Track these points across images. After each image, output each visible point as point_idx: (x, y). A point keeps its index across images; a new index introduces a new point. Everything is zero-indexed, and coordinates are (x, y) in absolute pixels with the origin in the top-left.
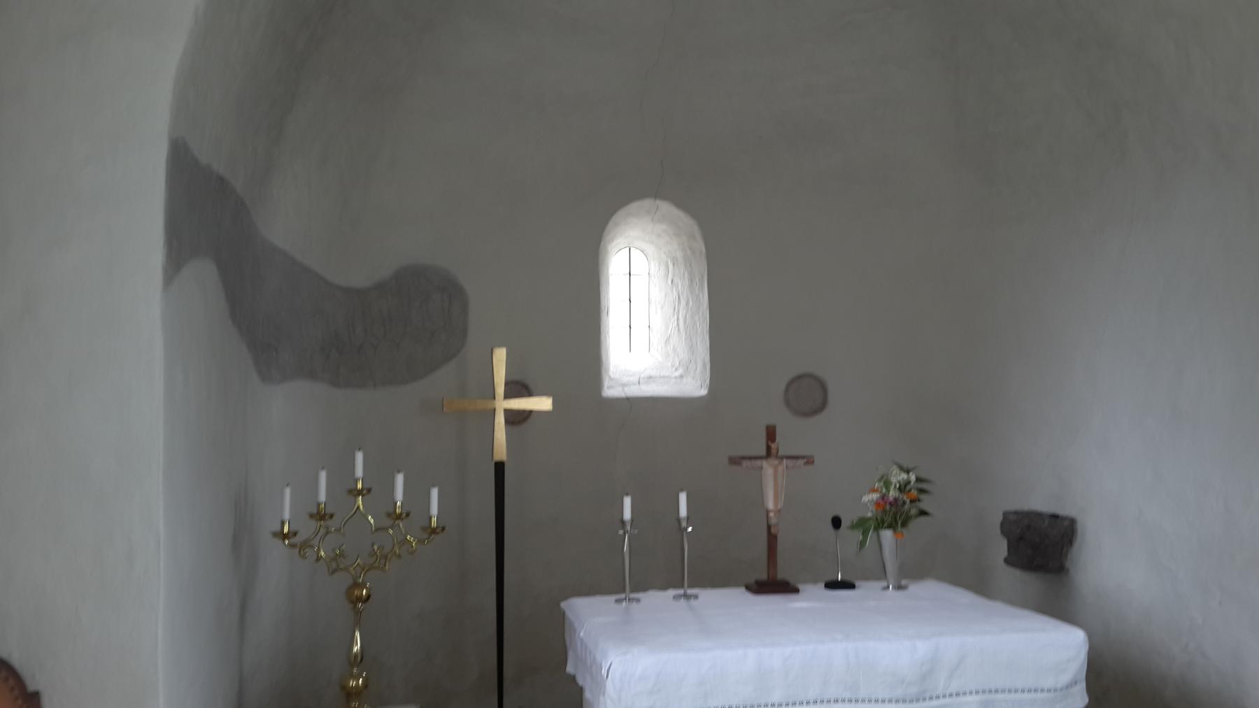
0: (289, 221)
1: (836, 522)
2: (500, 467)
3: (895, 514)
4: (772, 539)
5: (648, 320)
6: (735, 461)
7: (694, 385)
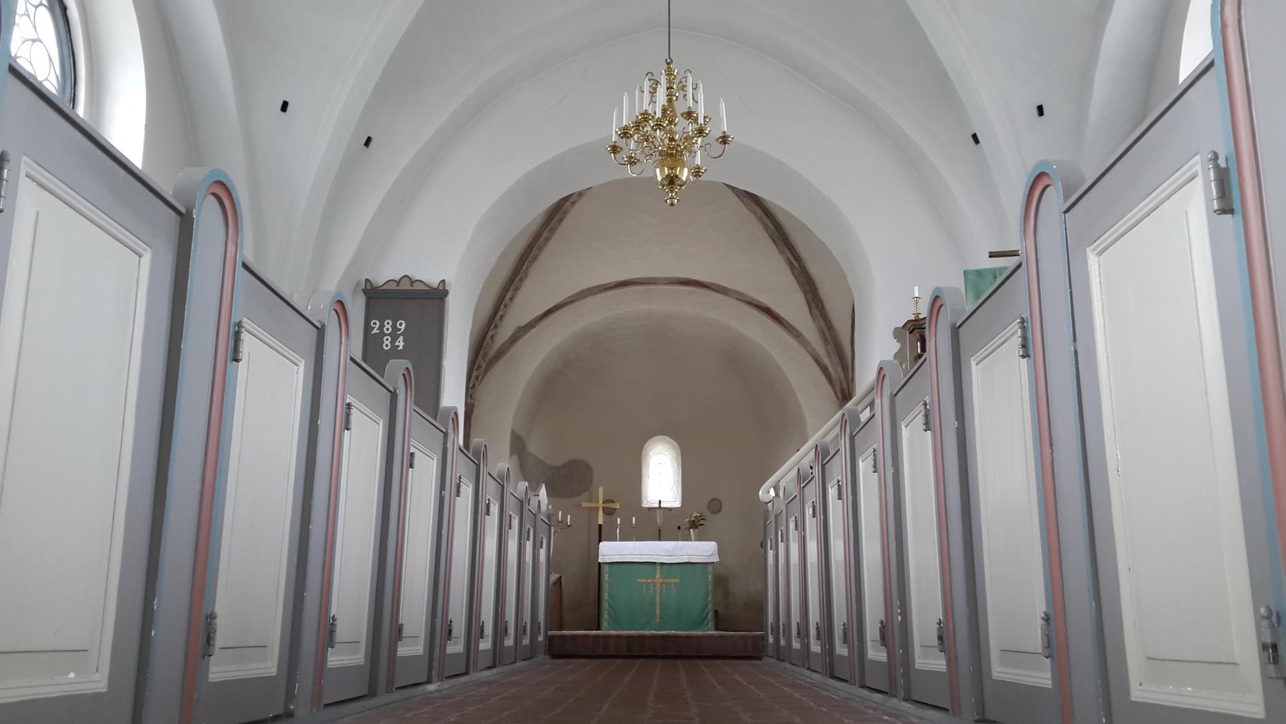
0: (535, 447)
5: (662, 478)
7: (677, 504)
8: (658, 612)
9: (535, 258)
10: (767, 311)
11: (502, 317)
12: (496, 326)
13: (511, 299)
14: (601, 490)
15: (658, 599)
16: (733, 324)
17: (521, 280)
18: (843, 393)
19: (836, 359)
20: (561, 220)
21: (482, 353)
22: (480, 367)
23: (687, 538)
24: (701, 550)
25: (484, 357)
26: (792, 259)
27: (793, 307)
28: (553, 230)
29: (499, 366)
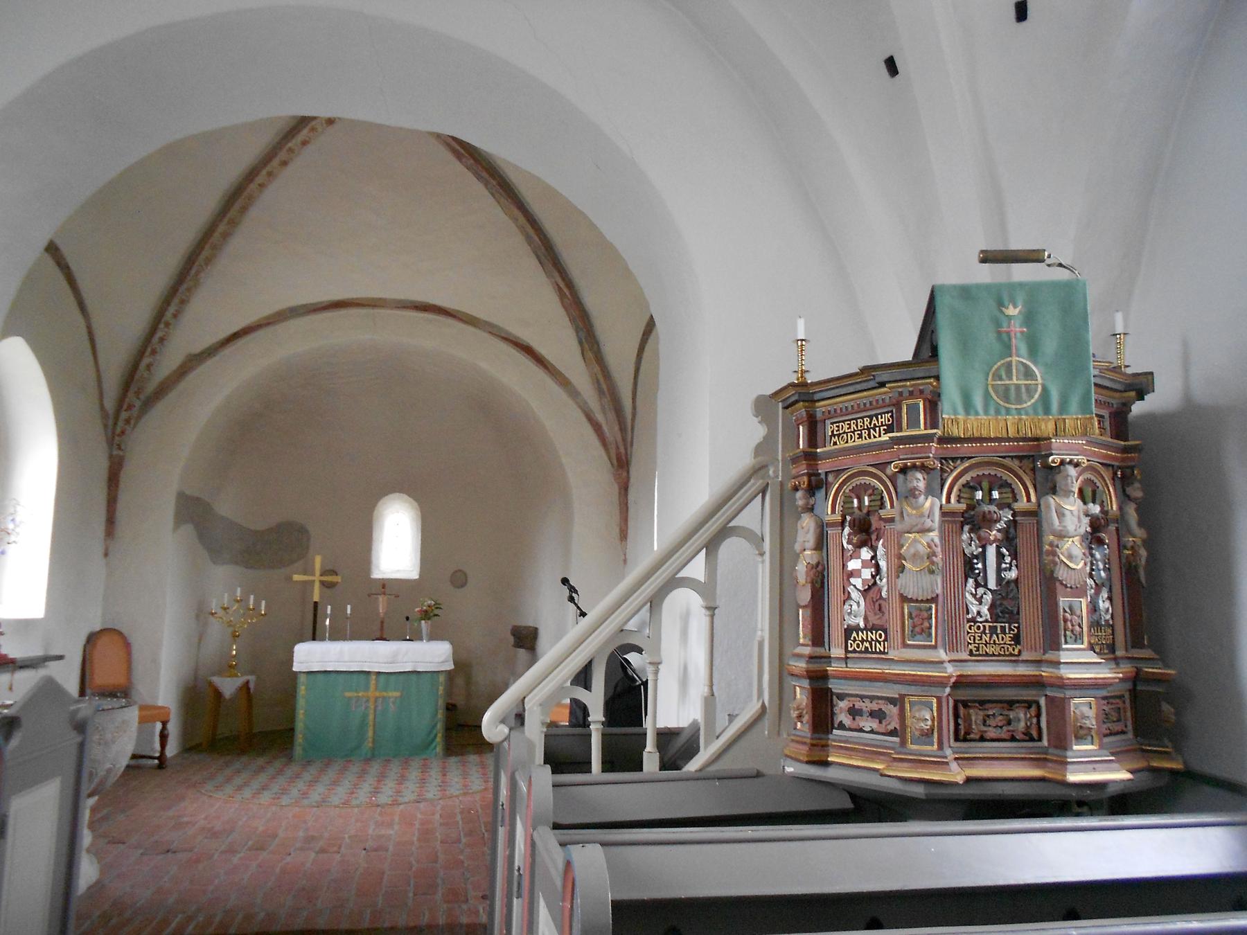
0: (227, 506)
1: (407, 619)
2: (316, 603)
3: (426, 615)
4: (382, 622)
5: (397, 544)
6: (11, 689)
7: (414, 575)
8: (370, 734)
9: (208, 261)
10: (528, 350)
11: (162, 340)
12: (154, 352)
13: (175, 316)
14: (318, 560)
15: (371, 717)
16: (484, 365)
17: (189, 290)
18: (619, 459)
19: (612, 416)
20: (244, 210)
21: (133, 389)
22: (130, 407)
23: (415, 637)
24: (431, 655)
25: (137, 393)
26: (562, 285)
27: (560, 343)
28: (234, 223)
29: (160, 407)
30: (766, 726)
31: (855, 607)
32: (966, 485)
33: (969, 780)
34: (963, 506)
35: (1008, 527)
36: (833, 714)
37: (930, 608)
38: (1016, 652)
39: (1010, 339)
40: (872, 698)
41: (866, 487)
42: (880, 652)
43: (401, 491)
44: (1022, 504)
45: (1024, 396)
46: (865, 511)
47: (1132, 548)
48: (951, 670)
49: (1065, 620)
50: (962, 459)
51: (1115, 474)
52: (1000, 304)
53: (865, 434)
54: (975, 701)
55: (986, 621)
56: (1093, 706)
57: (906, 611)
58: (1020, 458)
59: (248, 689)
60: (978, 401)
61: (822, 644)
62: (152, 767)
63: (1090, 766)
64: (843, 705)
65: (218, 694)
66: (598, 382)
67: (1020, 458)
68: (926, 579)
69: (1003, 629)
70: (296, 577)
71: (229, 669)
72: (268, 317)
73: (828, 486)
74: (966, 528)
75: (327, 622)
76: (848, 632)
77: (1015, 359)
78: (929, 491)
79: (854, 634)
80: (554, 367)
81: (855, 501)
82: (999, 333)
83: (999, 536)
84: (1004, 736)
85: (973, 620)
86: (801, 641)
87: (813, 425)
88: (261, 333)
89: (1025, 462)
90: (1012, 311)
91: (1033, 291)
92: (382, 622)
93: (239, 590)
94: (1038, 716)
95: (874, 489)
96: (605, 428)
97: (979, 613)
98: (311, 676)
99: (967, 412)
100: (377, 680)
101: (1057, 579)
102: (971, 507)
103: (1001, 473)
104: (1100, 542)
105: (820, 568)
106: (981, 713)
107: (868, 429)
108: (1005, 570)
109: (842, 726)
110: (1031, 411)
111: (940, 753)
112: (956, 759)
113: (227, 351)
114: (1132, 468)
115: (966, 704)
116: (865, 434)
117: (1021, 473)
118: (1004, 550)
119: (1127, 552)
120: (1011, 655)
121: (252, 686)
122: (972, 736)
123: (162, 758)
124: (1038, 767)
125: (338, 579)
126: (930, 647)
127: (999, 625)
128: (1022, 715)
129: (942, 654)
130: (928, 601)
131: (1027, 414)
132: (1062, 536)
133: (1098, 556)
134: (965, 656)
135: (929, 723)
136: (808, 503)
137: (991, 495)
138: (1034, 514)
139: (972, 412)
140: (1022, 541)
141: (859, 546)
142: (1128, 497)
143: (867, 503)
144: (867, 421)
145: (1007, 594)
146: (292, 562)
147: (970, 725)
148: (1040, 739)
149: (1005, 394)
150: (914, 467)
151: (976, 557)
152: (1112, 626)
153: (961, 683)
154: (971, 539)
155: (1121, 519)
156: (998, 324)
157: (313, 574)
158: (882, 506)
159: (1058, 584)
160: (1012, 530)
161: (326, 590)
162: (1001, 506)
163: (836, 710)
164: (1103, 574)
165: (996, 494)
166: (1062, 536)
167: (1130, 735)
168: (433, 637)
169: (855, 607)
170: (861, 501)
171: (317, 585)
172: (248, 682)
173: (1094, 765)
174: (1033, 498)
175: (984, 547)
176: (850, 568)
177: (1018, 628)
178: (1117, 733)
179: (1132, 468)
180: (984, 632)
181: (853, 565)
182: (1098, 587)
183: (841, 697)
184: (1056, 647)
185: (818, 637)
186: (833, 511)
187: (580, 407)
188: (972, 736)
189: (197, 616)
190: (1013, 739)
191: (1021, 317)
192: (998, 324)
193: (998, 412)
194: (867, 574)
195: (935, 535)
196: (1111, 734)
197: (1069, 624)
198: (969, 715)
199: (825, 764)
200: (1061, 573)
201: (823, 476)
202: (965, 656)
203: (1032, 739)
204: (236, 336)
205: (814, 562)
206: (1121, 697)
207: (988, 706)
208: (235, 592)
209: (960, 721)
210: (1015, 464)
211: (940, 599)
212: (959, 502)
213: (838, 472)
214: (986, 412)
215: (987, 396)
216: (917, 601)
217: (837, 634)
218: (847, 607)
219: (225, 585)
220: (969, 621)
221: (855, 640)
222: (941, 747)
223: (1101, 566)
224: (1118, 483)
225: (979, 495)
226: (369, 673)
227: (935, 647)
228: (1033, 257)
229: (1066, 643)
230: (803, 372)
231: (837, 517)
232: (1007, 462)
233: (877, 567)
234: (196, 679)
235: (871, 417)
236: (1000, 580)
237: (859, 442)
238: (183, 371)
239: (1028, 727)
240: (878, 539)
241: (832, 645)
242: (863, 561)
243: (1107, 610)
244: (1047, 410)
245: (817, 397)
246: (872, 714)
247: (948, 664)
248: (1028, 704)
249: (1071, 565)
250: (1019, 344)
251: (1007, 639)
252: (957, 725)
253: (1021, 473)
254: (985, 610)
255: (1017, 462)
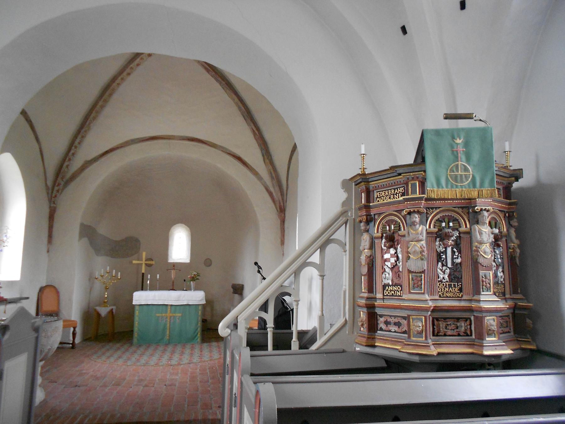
0: (103, 230)
1: (185, 280)
2: (143, 273)
3: (193, 279)
4: (173, 282)
5: (180, 247)
7: (188, 261)
8: (168, 333)
9: (94, 118)
10: (239, 159)
11: (73, 154)
12: (70, 160)
13: (79, 143)
14: (144, 254)
15: (168, 325)
16: (219, 166)
17: (85, 131)
18: (280, 208)
19: (277, 188)
20: (111, 95)
21: (60, 176)
22: (59, 185)
23: (188, 289)
24: (196, 297)
25: (62, 178)
26: (255, 129)
27: (254, 156)
28: (106, 101)
29: (73, 185)
30: (347, 329)
31: (387, 275)
32: (438, 220)
33: (439, 354)
34: (436, 230)
35: (457, 239)
36: (377, 324)
37: (422, 276)
38: (460, 296)
39: (458, 154)
40: (395, 317)
41: (392, 221)
42: (399, 296)
43: (182, 223)
44: (463, 229)
45: (464, 180)
46: (392, 232)
47: (513, 248)
48: (431, 304)
49: (483, 281)
50: (436, 208)
51: (505, 215)
52: (453, 138)
53: (392, 197)
54: (442, 318)
55: (447, 282)
56: (495, 320)
57: (411, 277)
58: (462, 208)
59: (113, 312)
60: (443, 182)
61: (372, 292)
62: (69, 348)
63: (494, 347)
64: (382, 319)
65: (99, 315)
66: (271, 173)
67: (462, 208)
68: (420, 263)
69: (454, 285)
70: (134, 262)
71: (104, 303)
72: (121, 144)
73: (375, 220)
74: (438, 239)
75: (148, 282)
76: (384, 286)
77: (460, 163)
78: (421, 223)
79: (387, 288)
80: (251, 166)
81: (388, 227)
82: (453, 151)
83: (453, 243)
84: (455, 334)
85: (441, 281)
86: (363, 291)
87: (368, 193)
88: (118, 151)
89: (464, 209)
90: (458, 141)
91: (468, 132)
92: (173, 282)
93: (108, 267)
94: (470, 325)
95: (396, 222)
96: (274, 194)
97: (443, 278)
98: (141, 307)
99: (438, 187)
100: (171, 308)
101: (479, 263)
102: (440, 230)
103: (454, 214)
104: (499, 246)
105: (372, 257)
106: (445, 323)
107: (393, 195)
108: (456, 258)
109: (381, 329)
110: (467, 187)
111: (426, 341)
112: (433, 344)
113: (103, 159)
114: (513, 212)
115: (437, 319)
116: (392, 197)
117: (462, 214)
118: (455, 250)
119: (511, 250)
120: (458, 297)
121: (114, 311)
122: (440, 334)
123: (73, 344)
124: (470, 348)
125: (153, 262)
126: (421, 293)
127: (452, 283)
128: (463, 324)
129: (427, 297)
130: (420, 272)
131: (465, 188)
132: (481, 243)
133: (497, 252)
134: (437, 297)
135: (421, 328)
136: (366, 228)
137: (449, 224)
138: (469, 233)
139: (441, 187)
140: (463, 245)
141: (389, 247)
142: (511, 226)
143: (393, 228)
144: (393, 191)
145: (456, 269)
146: (132, 255)
147: (440, 329)
148: (471, 335)
149: (455, 179)
150: (414, 212)
151: (442, 253)
152: (504, 284)
153: (436, 310)
154: (440, 245)
155: (508, 235)
156: (452, 147)
157: (142, 260)
158: (400, 229)
159: (479, 265)
160: (458, 240)
161: (147, 267)
162: (454, 229)
163: (379, 322)
164: (500, 260)
165: (451, 224)
166: (481, 243)
167: (512, 333)
168: (196, 289)
169: (387, 275)
170: (390, 227)
171: (144, 265)
172: (112, 309)
173: (496, 347)
174: (468, 226)
175: (446, 248)
176: (385, 258)
177: (461, 285)
178: (506, 333)
179: (513, 212)
180: (446, 287)
181: (387, 256)
182: (498, 266)
183: (381, 316)
184: (479, 293)
185: (371, 289)
186: (378, 232)
187: (263, 185)
188: (440, 334)
189: (89, 280)
190: (459, 335)
191: (462, 144)
192: (452, 147)
193: (452, 187)
194: (393, 260)
195: (423, 243)
196: (503, 333)
197: (484, 283)
198: (439, 324)
199: (374, 346)
200: (481, 260)
201: (373, 216)
202: (437, 297)
203: (467, 335)
204: (107, 152)
205: (369, 255)
206: (508, 316)
207: (447, 320)
208: (106, 268)
209: (435, 327)
210: (460, 211)
211: (426, 272)
212: (434, 227)
213: (380, 214)
214: (447, 187)
215: (447, 179)
216: (415, 273)
217: (379, 288)
218: (384, 275)
219: (102, 265)
220: (439, 281)
221: (387, 290)
222: (426, 339)
223: (499, 257)
224: (507, 219)
225: (444, 224)
226: (167, 305)
227: (424, 293)
228: (468, 116)
229: (483, 291)
230: (364, 169)
231: (379, 235)
232: (456, 209)
233: (398, 257)
234: (89, 308)
235: (395, 189)
236: (453, 263)
237: (389, 200)
238: (83, 168)
239: (466, 330)
240: (398, 244)
241: (377, 292)
242: (391, 255)
243: (502, 277)
244: (474, 186)
245: (370, 180)
246: (395, 324)
247: (429, 301)
248: (466, 319)
249: (485, 256)
250: (462, 156)
251: (456, 290)
252: (433, 329)
253: (462, 214)
254: (446, 277)
255: (461, 210)
